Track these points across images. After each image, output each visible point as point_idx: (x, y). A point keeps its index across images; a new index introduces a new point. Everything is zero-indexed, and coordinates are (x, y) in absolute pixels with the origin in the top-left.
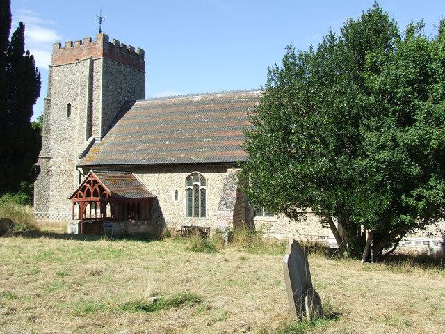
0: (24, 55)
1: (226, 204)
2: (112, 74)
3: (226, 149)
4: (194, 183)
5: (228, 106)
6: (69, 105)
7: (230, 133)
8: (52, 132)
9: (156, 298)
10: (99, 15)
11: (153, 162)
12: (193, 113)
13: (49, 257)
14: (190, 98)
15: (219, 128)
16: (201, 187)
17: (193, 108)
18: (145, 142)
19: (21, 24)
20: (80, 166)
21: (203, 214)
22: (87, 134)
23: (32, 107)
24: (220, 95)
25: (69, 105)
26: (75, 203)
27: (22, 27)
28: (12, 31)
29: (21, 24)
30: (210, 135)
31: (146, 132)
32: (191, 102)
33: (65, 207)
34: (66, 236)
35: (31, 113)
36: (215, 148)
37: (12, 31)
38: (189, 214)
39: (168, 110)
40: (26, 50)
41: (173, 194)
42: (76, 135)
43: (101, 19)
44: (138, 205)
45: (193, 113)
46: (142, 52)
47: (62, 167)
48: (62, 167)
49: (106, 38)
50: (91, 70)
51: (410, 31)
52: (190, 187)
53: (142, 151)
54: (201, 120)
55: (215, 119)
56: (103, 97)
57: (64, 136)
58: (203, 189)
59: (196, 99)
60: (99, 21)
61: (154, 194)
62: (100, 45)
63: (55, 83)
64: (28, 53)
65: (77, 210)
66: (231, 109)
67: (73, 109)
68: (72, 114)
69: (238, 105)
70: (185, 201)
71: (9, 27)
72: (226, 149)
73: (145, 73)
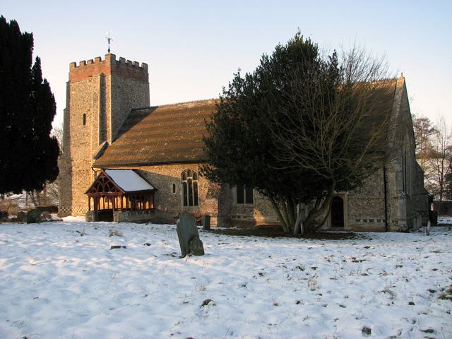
0: (43, 83)
1: (212, 194)
2: (119, 87)
4: (188, 178)
6: (85, 115)
8: (72, 139)
9: (72, 274)
12: (188, 118)
16: (193, 181)
17: (187, 114)
18: (148, 144)
20: (95, 167)
21: (196, 204)
22: (100, 139)
23: (51, 124)
24: (210, 102)
25: (85, 115)
26: (90, 198)
28: (33, 64)
35: (50, 133)
37: (33, 64)
38: (185, 204)
39: (166, 116)
40: (43, 79)
41: (172, 186)
42: (91, 140)
45: (188, 118)
46: (145, 66)
47: (81, 168)
48: (81, 168)
49: (113, 56)
50: (103, 85)
54: (193, 124)
56: (112, 107)
57: (82, 141)
61: (390, 71)
62: (108, 64)
63: (72, 97)
64: (45, 80)
65: (92, 204)
67: (87, 118)
68: (87, 123)
70: (181, 193)
71: (31, 63)
73: (148, 83)
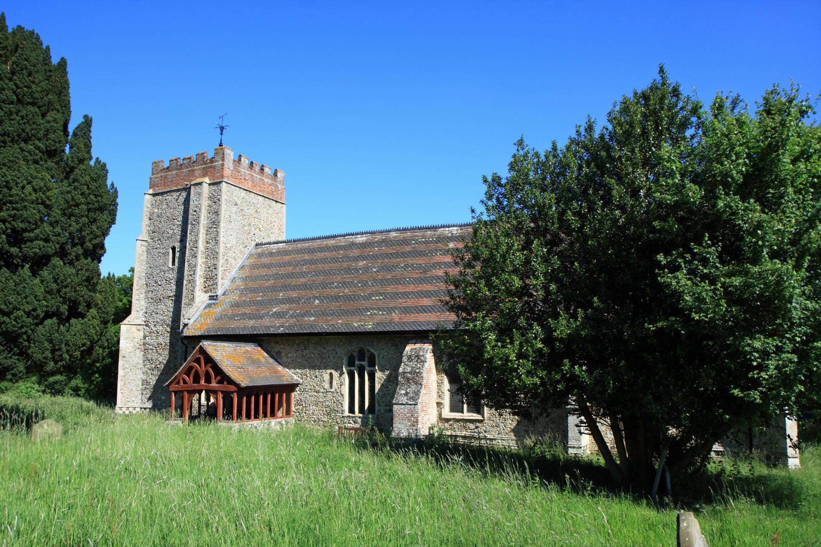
3: (406, 310)
5: (408, 249)
7: (411, 288)
10: (221, 124)
11: (296, 330)
12: (356, 259)
13: (268, 193)
14: (351, 239)
15: (397, 281)
17: (356, 252)
18: (283, 301)
19: (86, 117)
27: (88, 122)
29: (86, 117)
30: (382, 291)
31: (286, 287)
32: (352, 245)
33: (163, 398)
34: (226, 182)
36: (390, 310)
39: (319, 255)
43: (222, 128)
44: (454, 407)
51: (719, 108)
52: (362, 363)
53: (278, 315)
54: (366, 269)
55: (385, 268)
58: (361, 365)
59: (360, 239)
60: (219, 132)
66: (415, 253)
69: (422, 248)
72: (406, 310)
